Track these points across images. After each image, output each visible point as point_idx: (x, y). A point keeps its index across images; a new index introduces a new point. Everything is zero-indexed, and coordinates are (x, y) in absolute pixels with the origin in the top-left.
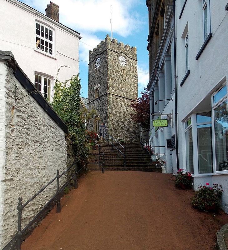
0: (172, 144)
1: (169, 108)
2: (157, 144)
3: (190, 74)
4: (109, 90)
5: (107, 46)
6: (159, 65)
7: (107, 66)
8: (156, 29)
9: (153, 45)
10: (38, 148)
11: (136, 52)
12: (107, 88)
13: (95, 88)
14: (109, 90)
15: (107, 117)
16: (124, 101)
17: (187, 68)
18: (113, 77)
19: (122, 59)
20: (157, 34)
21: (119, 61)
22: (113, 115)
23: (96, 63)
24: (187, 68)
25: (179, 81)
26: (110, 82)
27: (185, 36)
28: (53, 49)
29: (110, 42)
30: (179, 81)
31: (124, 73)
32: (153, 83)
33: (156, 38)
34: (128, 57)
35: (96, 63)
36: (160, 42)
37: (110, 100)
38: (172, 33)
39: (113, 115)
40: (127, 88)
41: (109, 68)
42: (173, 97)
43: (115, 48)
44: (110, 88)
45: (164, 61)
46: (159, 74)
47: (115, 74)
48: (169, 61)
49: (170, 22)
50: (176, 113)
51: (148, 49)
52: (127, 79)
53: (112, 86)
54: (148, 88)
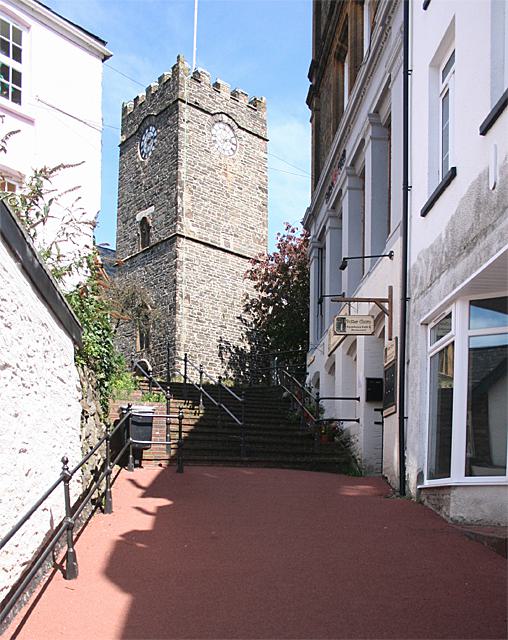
0: (383, 391)
1: (382, 279)
2: (337, 374)
3: (457, 179)
4: (181, 225)
5: (178, 91)
6: (345, 151)
7: (176, 150)
8: (337, 42)
9: (324, 91)
10: (10, 384)
11: (264, 115)
12: (175, 220)
13: (139, 218)
14: (181, 225)
15: (174, 308)
16: (225, 261)
17: (445, 162)
18: (194, 187)
19: (221, 132)
20: (340, 59)
21: (213, 138)
22: (195, 303)
23: (142, 140)
24: (445, 162)
25: (418, 200)
26: (185, 202)
27: (445, 64)
28: (24, 89)
29: (185, 79)
30: (418, 200)
31: (226, 175)
32: (325, 207)
33: (337, 71)
34: (239, 127)
35: (142, 140)
36: (373, 25)
37: (185, 256)
38: (400, 49)
39: (195, 303)
40: (235, 223)
41: (183, 155)
42: (396, 246)
43: (202, 98)
44: (185, 220)
45: (324, 227)
46: (345, 180)
47: (202, 177)
48: (384, 139)
49: (390, 18)
50: (405, 299)
51: (309, 102)
52: (235, 194)
53: (190, 214)
54: (309, 220)
